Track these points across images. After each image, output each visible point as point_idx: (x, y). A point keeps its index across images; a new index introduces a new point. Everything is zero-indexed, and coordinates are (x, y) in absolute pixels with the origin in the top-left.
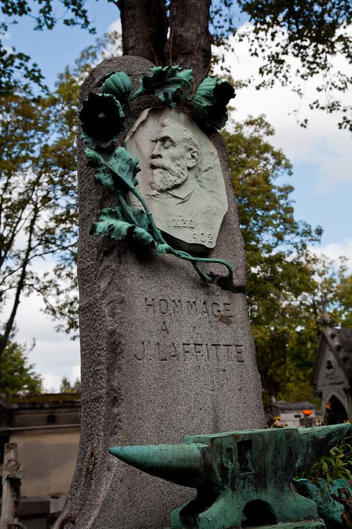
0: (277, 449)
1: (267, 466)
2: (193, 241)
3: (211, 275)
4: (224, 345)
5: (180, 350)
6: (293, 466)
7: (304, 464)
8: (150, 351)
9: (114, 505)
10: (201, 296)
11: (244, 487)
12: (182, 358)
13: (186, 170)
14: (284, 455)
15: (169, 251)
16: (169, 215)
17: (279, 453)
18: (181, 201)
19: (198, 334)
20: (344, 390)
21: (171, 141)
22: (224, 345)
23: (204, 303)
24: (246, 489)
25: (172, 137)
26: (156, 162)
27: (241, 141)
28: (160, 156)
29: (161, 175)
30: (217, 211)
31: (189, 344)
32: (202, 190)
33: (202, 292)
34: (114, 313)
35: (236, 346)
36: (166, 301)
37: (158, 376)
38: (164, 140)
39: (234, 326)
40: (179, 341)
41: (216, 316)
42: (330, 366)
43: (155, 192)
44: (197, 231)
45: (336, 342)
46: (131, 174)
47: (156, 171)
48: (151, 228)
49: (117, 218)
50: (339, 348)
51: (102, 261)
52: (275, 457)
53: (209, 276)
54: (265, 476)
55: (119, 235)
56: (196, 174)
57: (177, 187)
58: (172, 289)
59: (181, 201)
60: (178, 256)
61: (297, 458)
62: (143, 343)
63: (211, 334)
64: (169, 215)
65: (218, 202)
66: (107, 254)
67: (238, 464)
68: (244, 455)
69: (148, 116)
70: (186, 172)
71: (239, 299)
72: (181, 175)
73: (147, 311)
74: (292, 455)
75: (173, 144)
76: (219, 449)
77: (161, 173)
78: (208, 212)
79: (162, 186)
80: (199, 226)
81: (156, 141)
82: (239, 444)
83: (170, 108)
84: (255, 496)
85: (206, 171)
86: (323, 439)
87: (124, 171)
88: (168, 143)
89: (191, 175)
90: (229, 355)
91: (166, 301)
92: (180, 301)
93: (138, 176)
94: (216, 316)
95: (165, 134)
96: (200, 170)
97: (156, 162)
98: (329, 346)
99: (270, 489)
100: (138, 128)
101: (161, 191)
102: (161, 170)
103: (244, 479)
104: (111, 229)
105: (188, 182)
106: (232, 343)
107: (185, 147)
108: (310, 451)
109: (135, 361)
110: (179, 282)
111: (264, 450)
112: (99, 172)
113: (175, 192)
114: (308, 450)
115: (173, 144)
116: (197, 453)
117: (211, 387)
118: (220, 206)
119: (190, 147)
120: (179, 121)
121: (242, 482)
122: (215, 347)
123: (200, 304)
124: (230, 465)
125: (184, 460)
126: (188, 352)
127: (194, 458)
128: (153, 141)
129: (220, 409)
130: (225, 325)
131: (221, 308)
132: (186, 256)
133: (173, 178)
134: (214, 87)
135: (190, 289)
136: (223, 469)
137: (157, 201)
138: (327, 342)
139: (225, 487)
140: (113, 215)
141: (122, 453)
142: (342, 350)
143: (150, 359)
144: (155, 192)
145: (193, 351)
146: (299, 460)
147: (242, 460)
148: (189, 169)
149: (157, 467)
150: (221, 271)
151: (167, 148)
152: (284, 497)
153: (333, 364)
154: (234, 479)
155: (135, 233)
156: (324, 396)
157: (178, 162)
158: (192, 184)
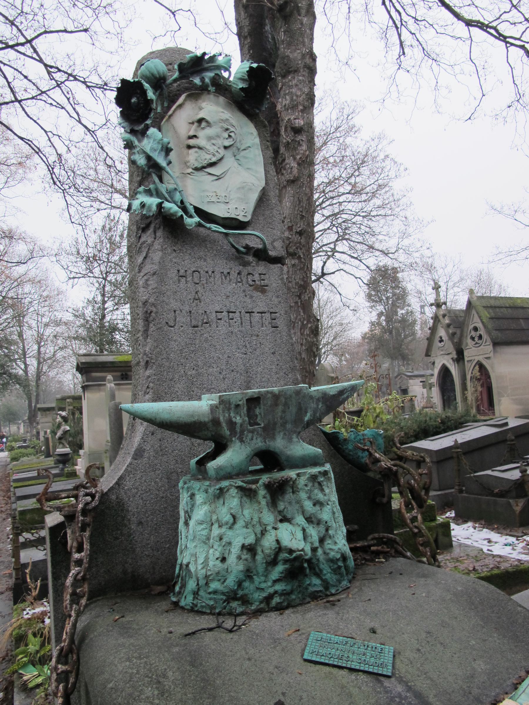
1: (276, 420)
2: (227, 215)
3: (247, 247)
4: (258, 313)
6: (302, 420)
7: (314, 418)
8: (182, 319)
9: (146, 455)
11: (252, 439)
12: (214, 325)
13: (223, 149)
14: (293, 409)
15: (199, 225)
16: (204, 191)
17: (289, 408)
18: (216, 178)
19: (232, 302)
20: (452, 359)
21: (207, 122)
22: (258, 313)
23: (239, 274)
24: (254, 441)
25: (208, 118)
26: (192, 142)
28: (195, 136)
29: (197, 155)
30: (253, 187)
31: (222, 312)
32: (240, 168)
34: (147, 285)
35: (271, 313)
36: (199, 272)
38: (200, 121)
39: (270, 294)
41: (251, 286)
42: (441, 341)
44: (232, 206)
45: (447, 321)
46: (163, 154)
47: (192, 151)
48: (183, 206)
49: (151, 195)
50: (448, 326)
51: (140, 237)
52: (284, 412)
53: (244, 248)
55: (150, 211)
56: (234, 153)
57: (212, 165)
58: (205, 260)
59: (216, 178)
60: (209, 229)
62: (175, 311)
63: (245, 302)
64: (204, 191)
65: (254, 178)
66: (144, 230)
67: (247, 419)
68: (254, 411)
69: (185, 100)
70: (222, 152)
72: (217, 154)
73: (179, 281)
74: (301, 410)
76: (227, 406)
77: (196, 152)
78: (243, 188)
80: (234, 201)
81: (193, 123)
83: (209, 92)
85: (245, 150)
86: (334, 395)
87: (155, 150)
88: (204, 124)
89: (228, 154)
90: (264, 322)
91: (199, 272)
92: (213, 272)
93: (172, 156)
94: (251, 286)
95: (201, 115)
96: (239, 149)
97: (192, 142)
98: (441, 324)
100: (174, 112)
101: (196, 169)
102: (196, 149)
103: (252, 432)
104: (143, 205)
105: (224, 160)
106: (266, 310)
107: (222, 127)
108: (320, 406)
109: (166, 328)
110: (212, 255)
112: (134, 153)
113: (209, 170)
114: (318, 406)
115: (209, 124)
118: (256, 182)
120: (217, 104)
122: (260, 314)
123: (234, 275)
124: (238, 420)
125: (192, 416)
126: (220, 319)
127: (203, 414)
128: (190, 123)
129: (253, 371)
131: (257, 277)
132: (217, 229)
133: (208, 157)
134: (248, 69)
135: (225, 261)
136: (231, 424)
137: (192, 179)
138: (439, 321)
139: (234, 439)
140: (149, 192)
141: (132, 410)
142: (451, 326)
143: (182, 326)
144: (190, 170)
146: (308, 415)
147: (251, 415)
148: (226, 148)
149: (166, 422)
150: (256, 244)
151: (203, 129)
152: (292, 447)
153: (443, 338)
154: (242, 432)
155: (164, 208)
156: (436, 365)
157: (214, 142)
158: (229, 162)
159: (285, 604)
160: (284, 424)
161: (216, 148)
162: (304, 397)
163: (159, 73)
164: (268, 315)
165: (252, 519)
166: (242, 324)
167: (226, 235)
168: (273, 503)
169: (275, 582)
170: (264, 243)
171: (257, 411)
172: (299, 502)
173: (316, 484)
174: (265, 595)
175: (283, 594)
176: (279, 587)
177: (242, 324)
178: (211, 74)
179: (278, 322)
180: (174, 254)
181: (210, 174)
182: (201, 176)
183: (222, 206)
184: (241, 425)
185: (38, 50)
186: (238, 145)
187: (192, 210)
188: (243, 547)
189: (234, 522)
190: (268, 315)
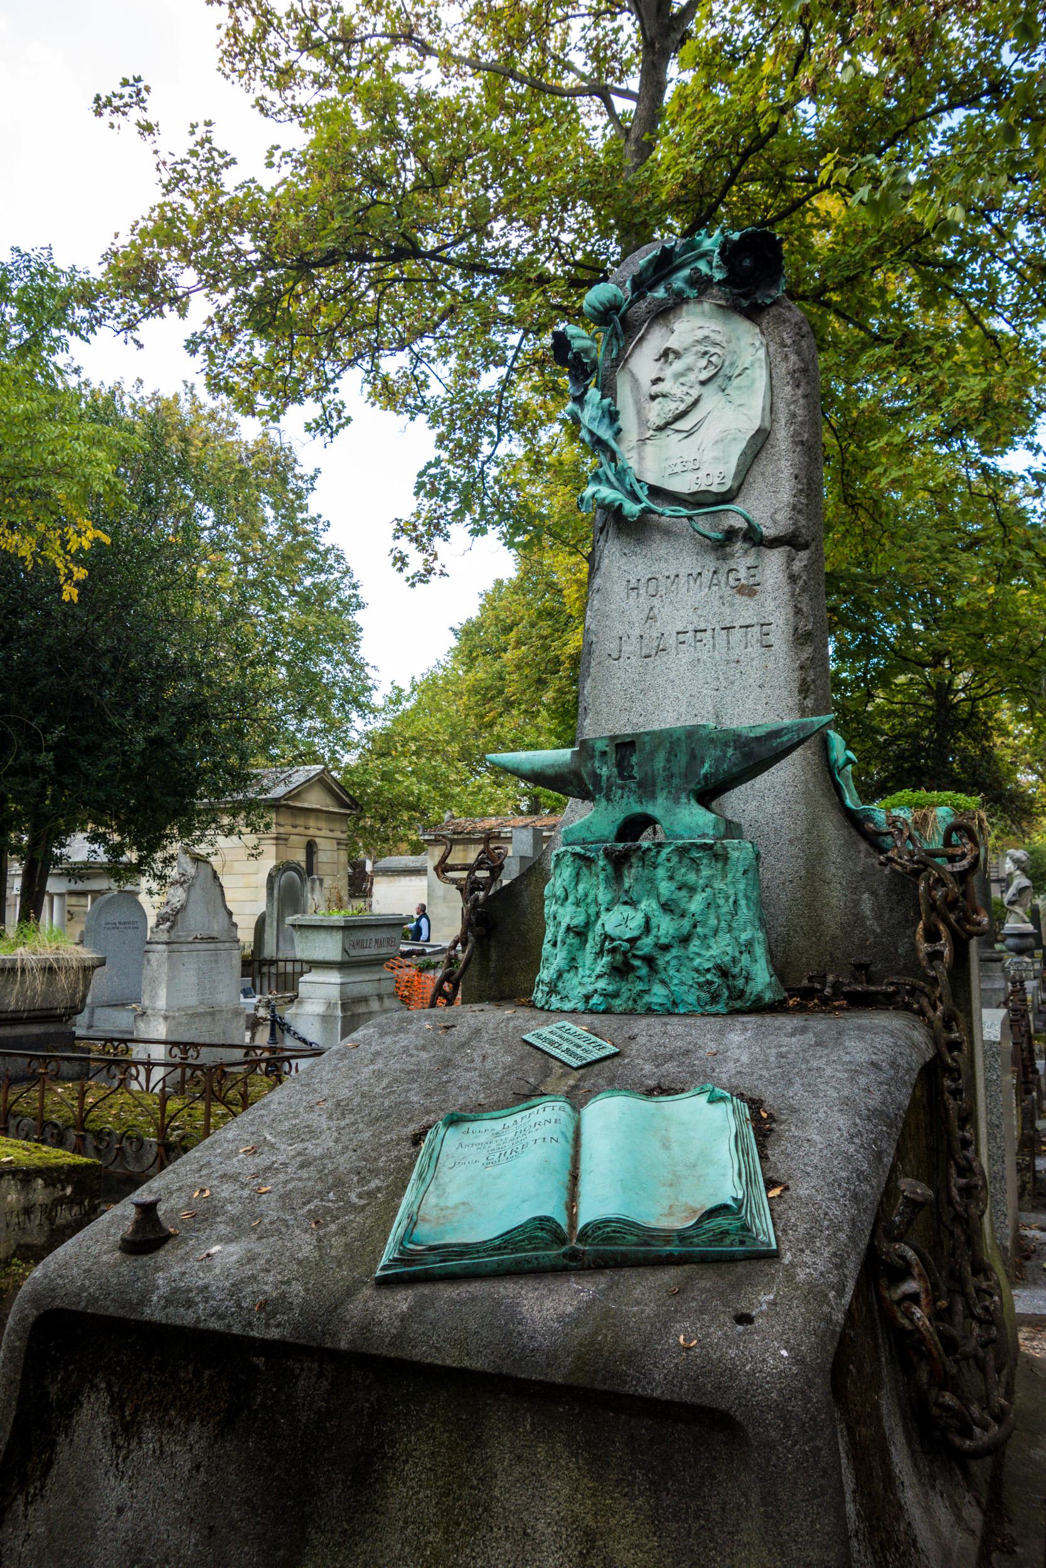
0: (672, 753)
2: (695, 489)
5: (672, 641)
10: (710, 562)
13: (698, 386)
14: (683, 759)
24: (625, 800)
25: (675, 346)
27: (60, 490)
33: (712, 557)
37: (637, 678)
40: (671, 630)
43: (651, 432)
46: (606, 421)
52: (668, 761)
54: (654, 784)
58: (666, 561)
61: (703, 763)
67: (615, 770)
71: (775, 560)
74: (695, 758)
75: (678, 355)
78: (722, 440)
79: (661, 422)
82: (617, 746)
83: (686, 301)
84: (637, 809)
88: (671, 356)
99: (660, 800)
101: (660, 429)
103: (623, 788)
106: (754, 621)
108: (729, 755)
111: (652, 754)
113: (676, 426)
116: (569, 756)
117: (715, 684)
119: (703, 349)
121: (620, 792)
123: (707, 575)
124: (604, 771)
125: (553, 766)
130: (745, 598)
131: (743, 574)
136: (596, 777)
144: (651, 432)
145: (692, 640)
146: (706, 765)
147: (623, 767)
148: (703, 383)
150: (739, 523)
154: (609, 788)
157: (682, 380)
159: (602, 1008)
160: (671, 777)
161: (685, 389)
162: (699, 739)
163: (601, 303)
164: (757, 629)
165: (586, 896)
166: (714, 646)
167: (690, 518)
168: (617, 877)
169: (599, 977)
170: (747, 520)
171: (634, 760)
172: (651, 881)
173: (686, 861)
174: (584, 991)
175: (606, 995)
176: (601, 984)
177: (714, 646)
178: (686, 272)
179: (772, 639)
180: (624, 560)
181: (678, 431)
182: (671, 439)
183: (691, 476)
184: (608, 778)
185: (645, 344)
186: (727, 371)
187: (643, 494)
188: (569, 929)
189: (566, 898)
190: (757, 629)
